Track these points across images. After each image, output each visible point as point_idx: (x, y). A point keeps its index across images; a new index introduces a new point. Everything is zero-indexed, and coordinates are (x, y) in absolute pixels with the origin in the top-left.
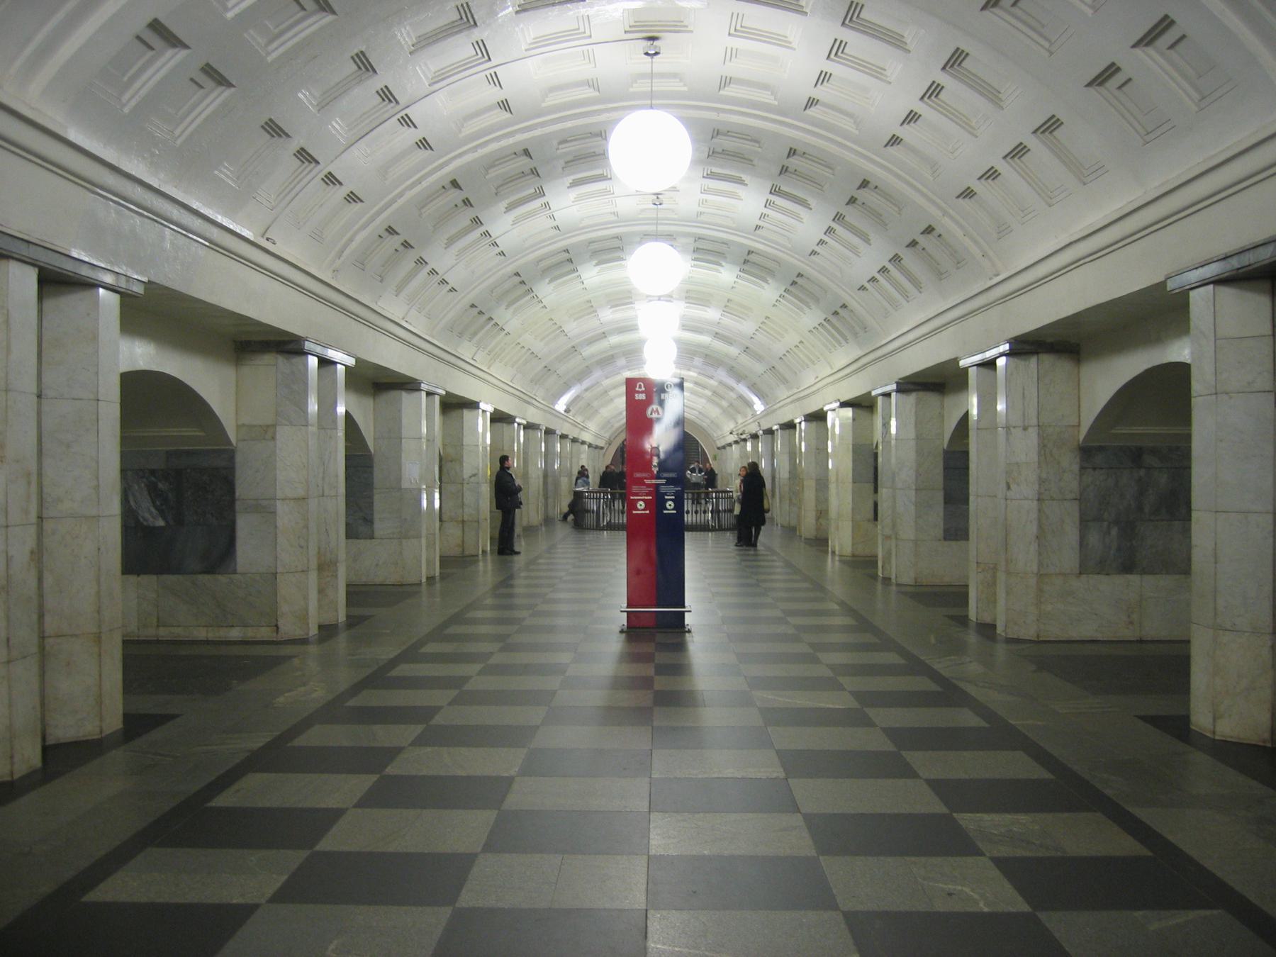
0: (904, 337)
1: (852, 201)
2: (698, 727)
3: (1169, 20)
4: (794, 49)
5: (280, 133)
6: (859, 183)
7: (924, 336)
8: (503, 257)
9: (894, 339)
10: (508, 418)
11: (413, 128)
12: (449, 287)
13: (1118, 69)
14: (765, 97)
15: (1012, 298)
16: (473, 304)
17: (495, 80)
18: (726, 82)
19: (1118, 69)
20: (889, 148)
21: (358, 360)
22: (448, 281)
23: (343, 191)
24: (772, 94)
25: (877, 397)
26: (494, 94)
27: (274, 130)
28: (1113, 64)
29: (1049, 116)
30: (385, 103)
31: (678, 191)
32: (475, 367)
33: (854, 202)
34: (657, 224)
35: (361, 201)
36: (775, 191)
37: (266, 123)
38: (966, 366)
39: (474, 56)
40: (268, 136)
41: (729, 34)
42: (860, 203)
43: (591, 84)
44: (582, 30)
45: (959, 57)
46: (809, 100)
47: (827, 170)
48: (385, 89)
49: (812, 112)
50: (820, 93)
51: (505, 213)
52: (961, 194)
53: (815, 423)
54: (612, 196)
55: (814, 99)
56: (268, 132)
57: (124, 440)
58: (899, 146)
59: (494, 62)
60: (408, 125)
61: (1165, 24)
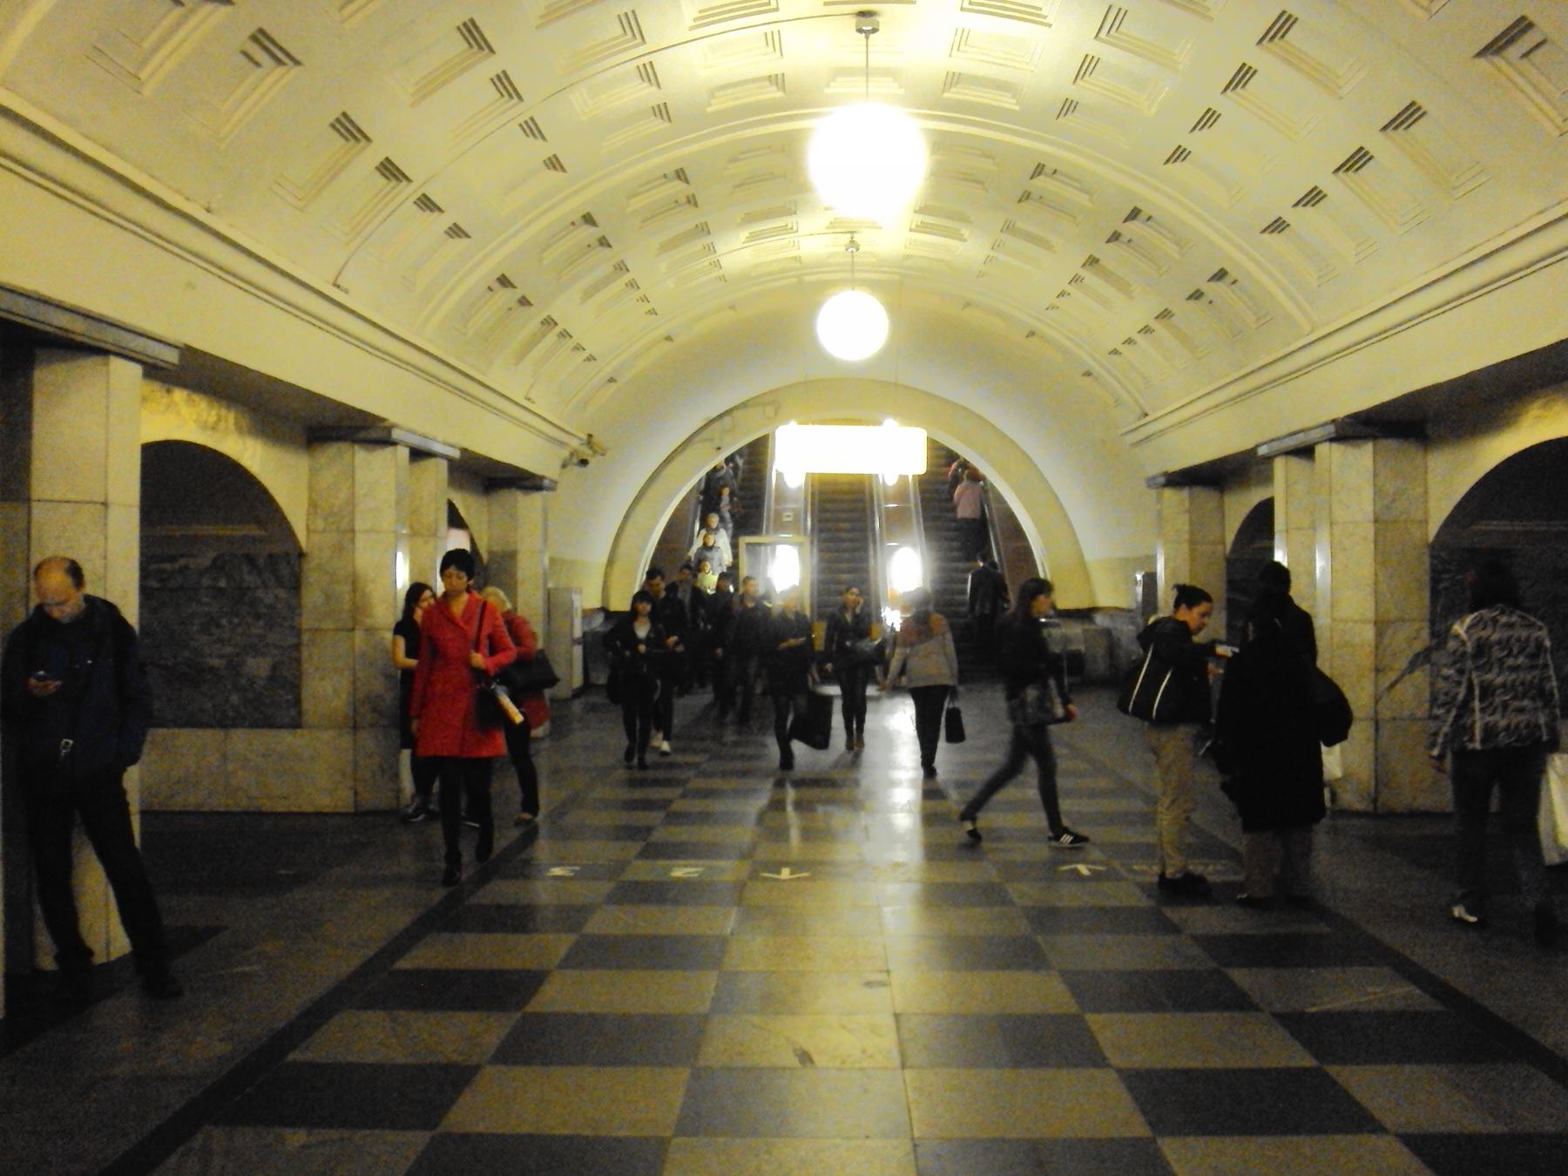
0: (1257, 375)
1: (1115, 237)
2: (812, 486)
3: (1527, 22)
4: (1050, 26)
5: (459, 233)
6: (1108, 235)
7: (1543, 259)
8: (654, 316)
9: (1319, 339)
10: (527, 479)
11: (540, 140)
12: (585, 354)
13: (1530, 25)
14: (1008, 102)
15: (1546, 266)
16: (611, 378)
17: (648, 74)
18: (954, 79)
19: (1530, 25)
20: (1170, 165)
21: (464, 451)
22: (370, 135)
23: (445, 221)
24: (1013, 97)
25: (1269, 459)
26: (645, 94)
27: (347, 128)
28: (1523, 18)
29: (1407, 103)
30: (503, 100)
31: (880, 228)
32: (530, 411)
33: (1117, 239)
34: (852, 271)
35: (297, 63)
36: (1009, 228)
37: (338, 120)
38: (1311, 442)
39: (620, 37)
40: (342, 141)
41: (962, 9)
42: (1126, 241)
43: (777, 80)
44: (790, 226)
45: (1210, 118)
46: (1066, 102)
47: (1083, 195)
48: (469, 24)
49: (1070, 120)
50: (1084, 92)
51: (537, 27)
52: (1268, 227)
53: (1368, 448)
54: (796, 234)
55: (1072, 101)
56: (342, 135)
57: (146, 541)
58: (1184, 163)
59: (718, 254)
60: (534, 135)
61: (1522, 26)
